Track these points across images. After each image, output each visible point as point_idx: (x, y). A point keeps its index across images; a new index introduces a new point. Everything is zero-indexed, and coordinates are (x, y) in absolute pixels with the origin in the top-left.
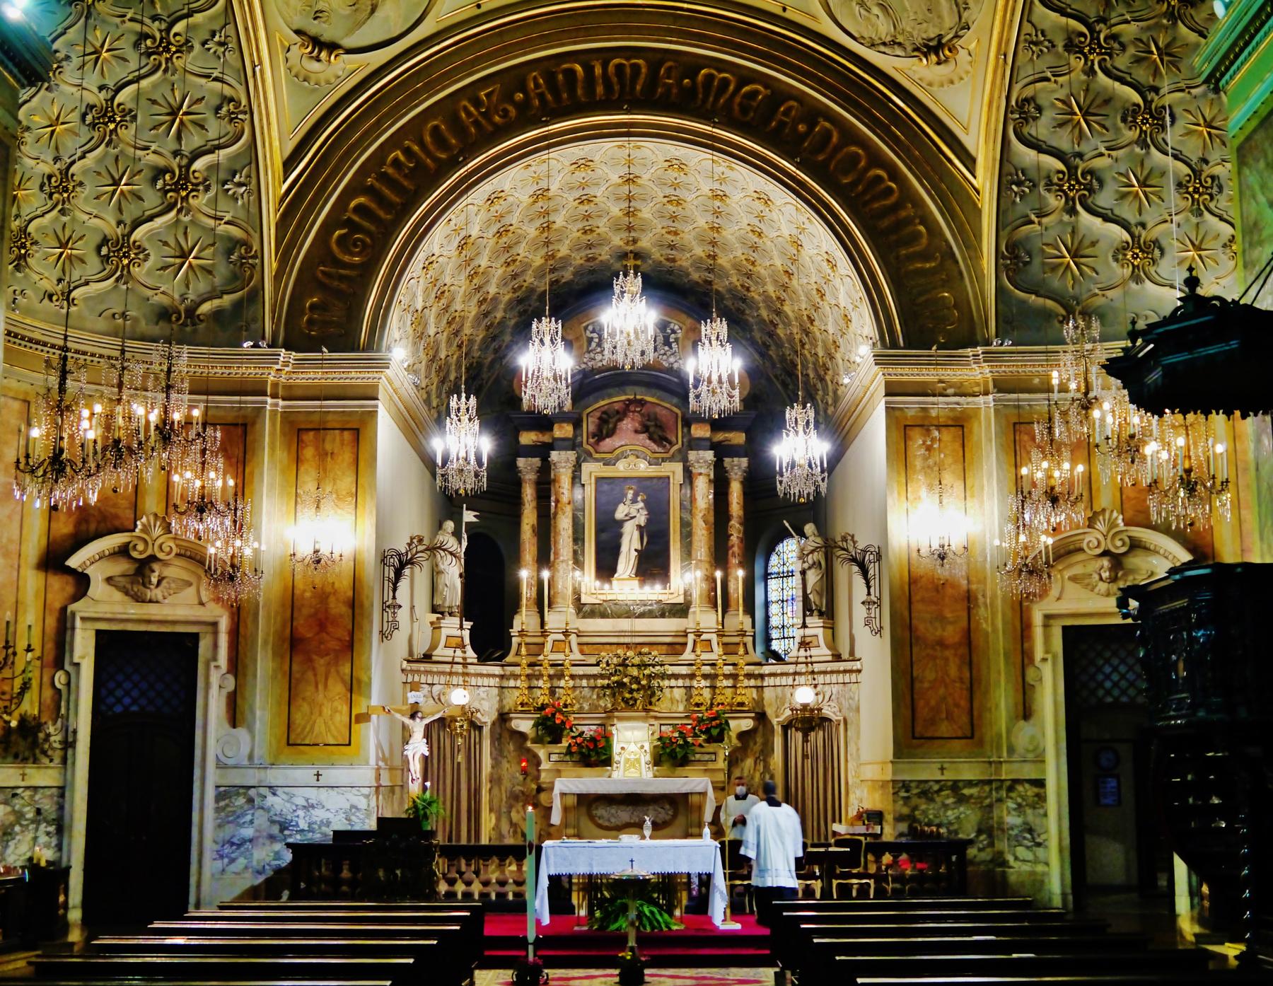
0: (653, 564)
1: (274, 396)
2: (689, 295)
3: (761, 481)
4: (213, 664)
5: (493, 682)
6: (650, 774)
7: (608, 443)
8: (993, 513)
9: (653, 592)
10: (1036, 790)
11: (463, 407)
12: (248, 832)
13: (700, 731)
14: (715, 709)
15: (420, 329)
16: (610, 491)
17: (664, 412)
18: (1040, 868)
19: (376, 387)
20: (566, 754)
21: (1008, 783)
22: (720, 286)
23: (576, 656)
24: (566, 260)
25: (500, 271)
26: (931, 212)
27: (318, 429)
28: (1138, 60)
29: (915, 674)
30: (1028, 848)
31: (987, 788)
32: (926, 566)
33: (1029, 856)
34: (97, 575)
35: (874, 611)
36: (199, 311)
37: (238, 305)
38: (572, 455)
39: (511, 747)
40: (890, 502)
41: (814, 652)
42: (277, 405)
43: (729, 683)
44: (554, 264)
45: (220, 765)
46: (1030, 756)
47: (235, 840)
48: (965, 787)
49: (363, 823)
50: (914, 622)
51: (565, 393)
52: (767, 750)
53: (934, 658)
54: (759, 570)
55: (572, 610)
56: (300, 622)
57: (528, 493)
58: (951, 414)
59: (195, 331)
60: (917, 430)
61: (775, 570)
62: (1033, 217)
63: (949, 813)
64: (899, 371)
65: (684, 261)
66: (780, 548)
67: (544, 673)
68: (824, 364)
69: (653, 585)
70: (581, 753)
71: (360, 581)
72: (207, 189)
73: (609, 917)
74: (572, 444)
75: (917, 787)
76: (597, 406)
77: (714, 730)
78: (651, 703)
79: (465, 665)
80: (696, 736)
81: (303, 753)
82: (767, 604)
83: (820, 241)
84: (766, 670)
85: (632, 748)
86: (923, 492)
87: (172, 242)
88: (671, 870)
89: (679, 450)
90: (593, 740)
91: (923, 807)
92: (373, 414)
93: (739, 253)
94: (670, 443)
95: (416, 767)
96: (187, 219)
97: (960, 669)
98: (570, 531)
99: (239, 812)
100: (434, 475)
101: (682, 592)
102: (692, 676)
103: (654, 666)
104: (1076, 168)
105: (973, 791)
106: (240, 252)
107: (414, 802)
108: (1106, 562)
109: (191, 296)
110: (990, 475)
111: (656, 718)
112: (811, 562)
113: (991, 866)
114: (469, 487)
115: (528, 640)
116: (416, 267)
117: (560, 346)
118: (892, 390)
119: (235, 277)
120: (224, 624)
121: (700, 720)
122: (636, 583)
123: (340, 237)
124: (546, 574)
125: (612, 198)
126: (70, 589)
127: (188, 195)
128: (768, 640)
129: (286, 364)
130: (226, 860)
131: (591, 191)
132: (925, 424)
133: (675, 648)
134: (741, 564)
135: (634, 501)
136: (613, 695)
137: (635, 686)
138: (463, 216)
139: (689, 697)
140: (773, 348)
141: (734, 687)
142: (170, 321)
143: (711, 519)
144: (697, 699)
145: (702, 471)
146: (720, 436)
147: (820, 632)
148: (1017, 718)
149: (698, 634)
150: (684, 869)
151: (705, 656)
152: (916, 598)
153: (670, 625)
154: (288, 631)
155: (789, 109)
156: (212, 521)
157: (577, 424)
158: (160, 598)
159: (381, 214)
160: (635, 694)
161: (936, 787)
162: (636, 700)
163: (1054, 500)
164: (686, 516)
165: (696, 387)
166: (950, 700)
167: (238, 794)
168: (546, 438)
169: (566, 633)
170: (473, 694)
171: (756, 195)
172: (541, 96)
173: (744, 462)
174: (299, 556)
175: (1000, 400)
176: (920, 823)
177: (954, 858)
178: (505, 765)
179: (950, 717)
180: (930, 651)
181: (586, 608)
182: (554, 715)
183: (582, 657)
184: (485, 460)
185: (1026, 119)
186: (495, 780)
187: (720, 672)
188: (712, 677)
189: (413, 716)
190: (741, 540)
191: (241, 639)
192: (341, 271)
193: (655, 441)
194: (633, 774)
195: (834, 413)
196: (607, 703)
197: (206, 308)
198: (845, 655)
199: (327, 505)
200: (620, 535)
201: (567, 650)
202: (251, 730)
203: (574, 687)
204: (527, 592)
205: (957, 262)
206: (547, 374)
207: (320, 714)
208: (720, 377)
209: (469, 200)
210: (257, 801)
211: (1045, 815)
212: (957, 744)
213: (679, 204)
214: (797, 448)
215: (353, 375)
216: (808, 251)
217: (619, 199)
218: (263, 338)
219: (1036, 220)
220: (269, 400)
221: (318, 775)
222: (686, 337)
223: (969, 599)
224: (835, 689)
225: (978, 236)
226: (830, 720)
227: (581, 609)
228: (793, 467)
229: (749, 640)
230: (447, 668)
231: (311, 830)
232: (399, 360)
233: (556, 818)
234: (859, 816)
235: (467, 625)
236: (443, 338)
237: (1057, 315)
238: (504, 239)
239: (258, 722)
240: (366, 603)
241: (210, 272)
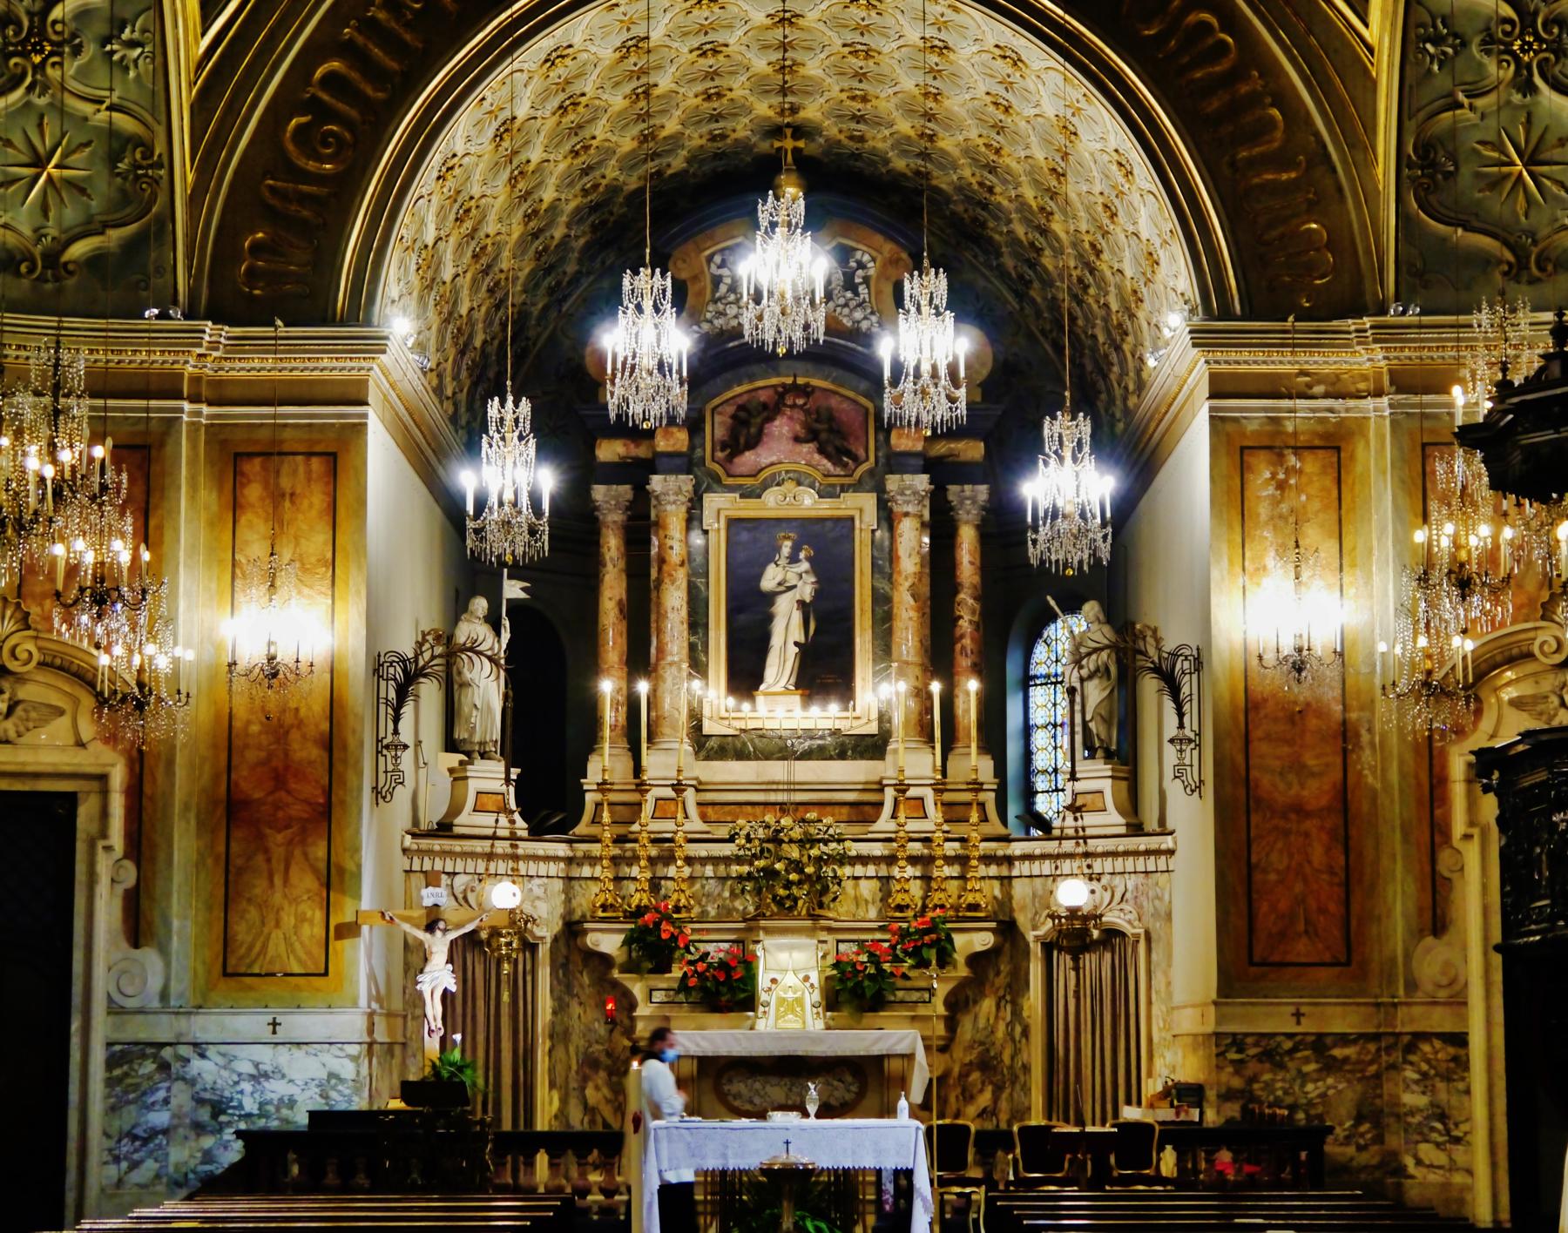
0: (825, 670)
1: (195, 399)
3: (1006, 528)
4: (101, 844)
5: (554, 869)
6: (820, 1024)
7: (748, 459)
8: (1386, 595)
9: (825, 716)
10: (1451, 1050)
11: (509, 417)
12: (160, 1118)
13: (905, 951)
14: (930, 914)
15: (429, 275)
16: (751, 544)
17: (845, 405)
18: (1458, 1178)
19: (363, 384)
20: (678, 991)
21: (1406, 1039)
22: (943, 180)
23: (695, 824)
24: (676, 140)
25: (562, 166)
26: (1294, 87)
27: (271, 454)
29: (1254, 859)
30: (1438, 1145)
31: (1372, 1047)
32: (1274, 681)
33: (1441, 1158)
35: (1190, 756)
36: (66, 257)
37: (133, 247)
38: (685, 482)
39: (586, 979)
40: (1215, 574)
41: (1089, 819)
42: (199, 414)
43: (954, 870)
45: (115, 1010)
46: (1442, 995)
47: (139, 1131)
48: (1335, 1046)
49: (350, 1102)
50: (1254, 774)
51: (679, 396)
52: (1018, 985)
53: (1286, 833)
54: (1012, 671)
55: (687, 747)
56: (242, 773)
57: (612, 545)
58: (1320, 428)
59: (59, 291)
60: (1263, 455)
61: (1042, 670)
62: (1461, 97)
63: (1310, 1087)
64: (1233, 356)
65: (879, 140)
67: (642, 853)
68: (1120, 325)
69: (825, 703)
70: (703, 989)
71: (342, 707)
72: (77, 51)
74: (685, 463)
75: (1256, 1045)
76: (729, 394)
78: (821, 905)
80: (897, 960)
81: (251, 988)
82: (1027, 730)
83: (1104, 134)
84: (1017, 849)
85: (790, 980)
86: (1270, 560)
87: (18, 139)
88: (848, 1164)
89: (871, 472)
90: (723, 965)
91: (1267, 1077)
92: (359, 429)
93: (973, 134)
94: (855, 459)
95: (434, 1009)
96: (42, 101)
97: (1328, 850)
98: (684, 613)
99: (145, 1086)
101: (874, 715)
102: (891, 860)
103: (826, 842)
104: (1536, 13)
105: (1350, 1051)
106: (132, 160)
107: (434, 1066)
110: (1383, 530)
111: (830, 930)
112: (1092, 667)
113: (1378, 1174)
114: (520, 551)
115: (613, 797)
119: (125, 198)
120: (118, 777)
121: (904, 934)
122: (796, 699)
123: (299, 127)
124: (643, 687)
125: (755, 46)
127: (44, 61)
128: (1029, 793)
129: (214, 346)
130: (124, 1165)
132: (1275, 444)
133: (864, 811)
134: (977, 670)
135: (793, 559)
136: (758, 891)
137: (793, 877)
138: (506, 90)
139: (886, 894)
140: (1036, 285)
141: (962, 877)
142: (18, 274)
143: (925, 590)
144: (899, 899)
145: (910, 508)
147: (1106, 785)
148: (1420, 934)
149: (902, 788)
151: (913, 825)
152: (1257, 733)
154: (223, 787)
158: (12, 734)
160: (795, 890)
161: (1288, 1045)
162: (796, 900)
163: (1464, 585)
164: (883, 585)
165: (895, 382)
166: (1312, 904)
167: (144, 1056)
168: (642, 451)
169: (678, 787)
171: (998, 52)
173: (982, 491)
174: (241, 667)
175: (1401, 405)
176: (1261, 1103)
177: (1303, 1155)
178: (576, 1009)
180: (1282, 823)
181: (712, 743)
182: (657, 925)
183: (705, 827)
184: (546, 506)
186: (559, 1035)
187: (939, 852)
189: (430, 928)
190: (977, 626)
191: (145, 802)
192: (304, 188)
193: (828, 457)
194: (791, 1023)
195: (1138, 406)
196: (747, 904)
197: (78, 250)
198: (1151, 824)
200: (769, 618)
201: (680, 816)
202: (164, 951)
203: (692, 878)
204: (611, 715)
205: (1334, 170)
207: (278, 925)
208: (934, 368)
209: (516, 65)
210: (176, 1067)
211: (1468, 1092)
212: (1324, 974)
213: (868, 56)
214: (1067, 484)
215: (326, 363)
216: (1087, 145)
217: (765, 47)
218: (175, 302)
219: (1466, 101)
220: (187, 406)
221: (274, 1024)
223: (1346, 736)
224: (1131, 882)
225: (1371, 129)
226: (1123, 935)
227: (705, 746)
228: (1055, 516)
229: (989, 798)
230: (481, 846)
231: (263, 1114)
232: (402, 335)
234: (1166, 1094)
237: (1500, 262)
238: (571, 117)
239: (175, 938)
240: (352, 742)
241: (83, 191)
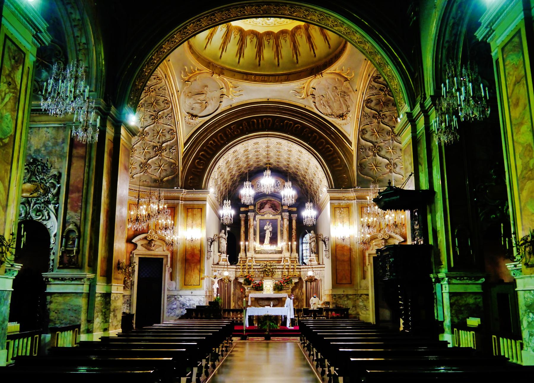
0: (274, 240)
1: (181, 200)
2: (283, 173)
3: (300, 220)
5: (234, 270)
7: (262, 211)
9: (273, 248)
12: (175, 306)
16: (263, 222)
18: (368, 316)
19: (206, 198)
22: (290, 171)
23: (254, 263)
24: (252, 165)
28: (390, 120)
32: (340, 242)
33: (365, 313)
34: (139, 244)
35: (327, 253)
37: (173, 178)
38: (253, 214)
41: (312, 262)
43: (292, 270)
44: (249, 166)
45: (168, 290)
54: (300, 242)
57: (243, 223)
65: (281, 165)
66: (306, 236)
72: (166, 151)
73: (262, 326)
74: (253, 211)
77: (288, 281)
79: (227, 266)
82: (302, 250)
83: (314, 162)
84: (302, 267)
85: (268, 286)
86: (339, 223)
90: (258, 284)
92: (205, 205)
95: (215, 290)
100: (220, 219)
102: (283, 269)
105: (351, 297)
106: (173, 166)
108: (383, 241)
109: (162, 176)
116: (216, 169)
117: (251, 188)
118: (331, 199)
120: (169, 256)
121: (285, 280)
122: (269, 245)
123: (198, 162)
124: (247, 243)
126: (133, 247)
128: (303, 259)
129: (184, 193)
131: (258, 149)
133: (279, 261)
134: (296, 241)
135: (269, 225)
143: (288, 229)
146: (290, 209)
148: (362, 279)
150: (280, 314)
152: (337, 250)
153: (278, 256)
155: (306, 131)
156: (168, 231)
157: (255, 205)
159: (208, 156)
163: (369, 227)
168: (247, 209)
169: (252, 258)
170: (229, 273)
172: (246, 127)
173: (296, 215)
178: (237, 290)
179: (346, 279)
185: (364, 134)
186: (234, 294)
188: (288, 269)
189: (215, 278)
194: (268, 293)
196: (262, 275)
198: (321, 263)
199: (194, 228)
204: (242, 248)
206: (248, 195)
214: (308, 213)
222: (282, 184)
223: (350, 250)
229: (297, 260)
230: (223, 266)
233: (249, 304)
235: (228, 256)
236: (222, 185)
